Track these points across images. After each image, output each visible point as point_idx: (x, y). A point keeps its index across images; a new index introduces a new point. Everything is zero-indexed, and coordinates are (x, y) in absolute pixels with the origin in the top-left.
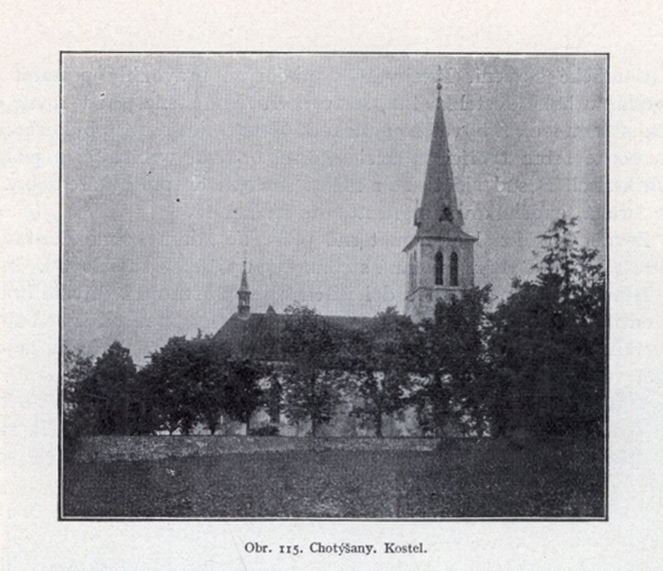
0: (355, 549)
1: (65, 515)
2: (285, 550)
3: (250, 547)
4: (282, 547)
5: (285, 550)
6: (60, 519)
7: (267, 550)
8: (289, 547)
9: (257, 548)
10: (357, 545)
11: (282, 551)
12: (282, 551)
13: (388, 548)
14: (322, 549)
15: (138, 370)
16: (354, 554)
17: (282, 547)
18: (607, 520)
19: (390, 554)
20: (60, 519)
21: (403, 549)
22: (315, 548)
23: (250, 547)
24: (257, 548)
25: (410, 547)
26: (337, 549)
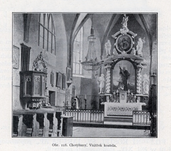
0: (82, 145)
1: (156, 14)
2: (63, 145)
3: (53, 145)
4: (62, 145)
5: (63, 145)
6: (157, 13)
7: (58, 145)
8: (64, 145)
9: (55, 145)
10: (82, 144)
11: (62, 146)
12: (62, 146)
13: (101, 146)
14: (73, 145)
15: (91, 78)
16: (82, 147)
17: (62, 145)
18: (157, 137)
19: (105, 147)
20: (157, 13)
21: (109, 146)
22: (71, 145)
23: (53, 145)
24: (55, 145)
25: (76, 145)
26: (77, 145)
